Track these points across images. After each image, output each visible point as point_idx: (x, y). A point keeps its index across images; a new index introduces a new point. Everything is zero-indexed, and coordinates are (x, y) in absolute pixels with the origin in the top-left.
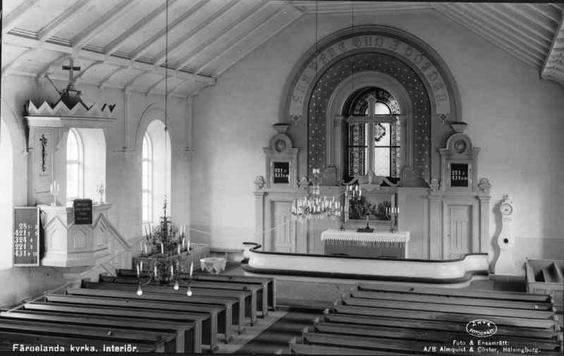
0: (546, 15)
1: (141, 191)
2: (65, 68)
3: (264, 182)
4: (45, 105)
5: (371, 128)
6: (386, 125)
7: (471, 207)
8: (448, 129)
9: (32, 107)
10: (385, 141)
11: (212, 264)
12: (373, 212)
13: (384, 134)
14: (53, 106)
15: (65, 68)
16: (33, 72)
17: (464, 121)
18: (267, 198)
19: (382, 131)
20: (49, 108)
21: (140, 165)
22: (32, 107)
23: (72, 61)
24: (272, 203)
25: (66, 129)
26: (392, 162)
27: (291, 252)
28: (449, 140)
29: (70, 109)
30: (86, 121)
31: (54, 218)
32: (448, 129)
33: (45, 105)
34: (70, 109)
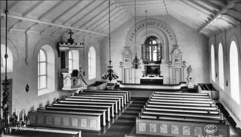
0: (212, 14)
1: (88, 67)
2: (69, 33)
3: (171, 54)
4: (64, 44)
5: (152, 48)
6: (156, 47)
7: (181, 69)
8: (174, 48)
9: (60, 44)
10: (155, 51)
11: (111, 88)
12: (153, 72)
13: (155, 49)
14: (66, 44)
15: (69, 33)
16: (201, 22)
17: (178, 45)
18: (123, 68)
19: (155, 48)
20: (65, 44)
21: (88, 59)
22: (60, 44)
23: (71, 31)
24: (125, 69)
25: (69, 50)
26: (158, 57)
27: (132, 83)
28: (174, 51)
29: (141, 79)
30: (75, 48)
31: (67, 76)
32: (174, 48)
33: (64, 44)
34: (141, 79)
